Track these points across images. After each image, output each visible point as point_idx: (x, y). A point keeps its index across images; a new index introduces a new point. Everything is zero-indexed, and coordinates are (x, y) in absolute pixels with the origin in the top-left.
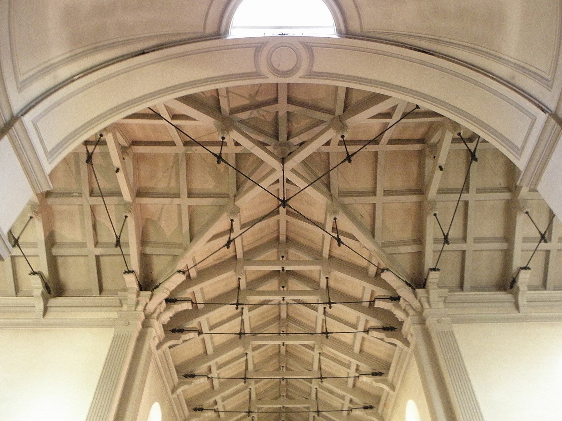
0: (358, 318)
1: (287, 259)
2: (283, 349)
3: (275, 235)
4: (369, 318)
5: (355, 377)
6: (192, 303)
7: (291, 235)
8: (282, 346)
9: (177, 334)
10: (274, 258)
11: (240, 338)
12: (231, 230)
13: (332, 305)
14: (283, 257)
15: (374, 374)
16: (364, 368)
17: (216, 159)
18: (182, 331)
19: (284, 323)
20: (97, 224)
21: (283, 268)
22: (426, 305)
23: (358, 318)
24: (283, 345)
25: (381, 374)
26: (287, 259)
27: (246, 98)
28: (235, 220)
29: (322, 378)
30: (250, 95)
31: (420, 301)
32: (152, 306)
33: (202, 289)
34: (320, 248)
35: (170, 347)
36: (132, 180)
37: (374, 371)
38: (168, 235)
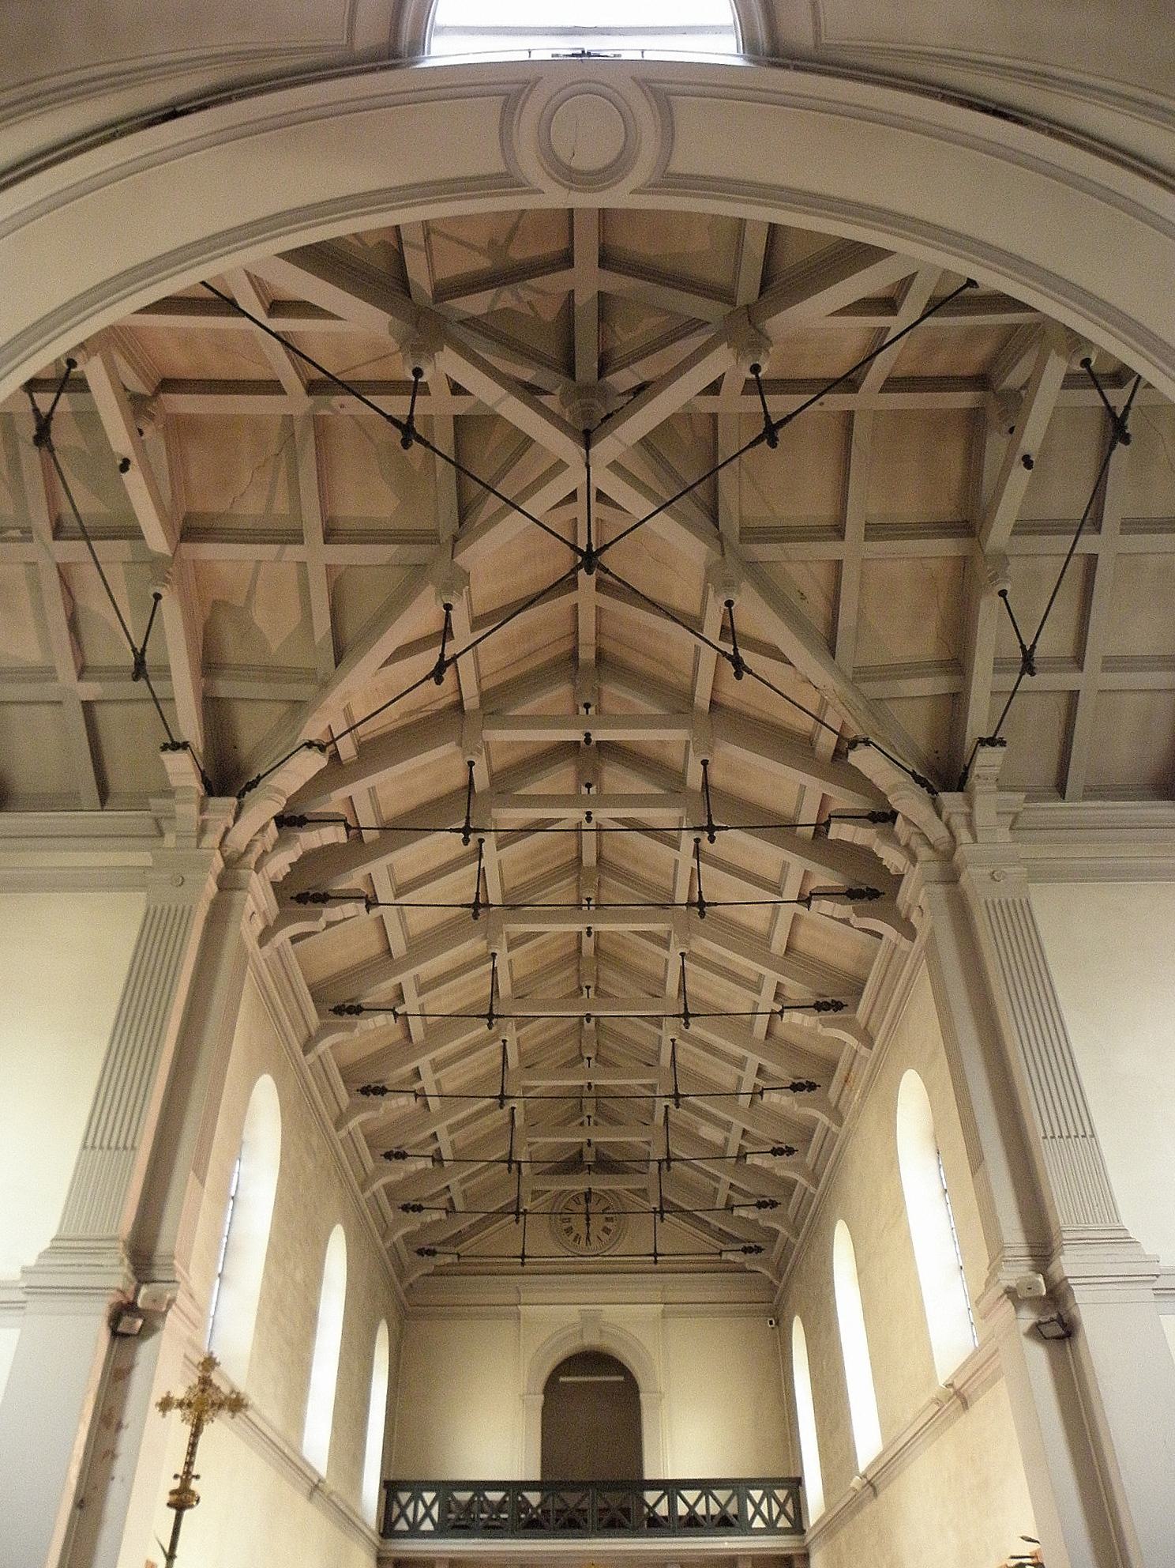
0: (785, 866)
1: (600, 789)
2: (588, 944)
3: (567, 646)
4: (812, 866)
5: (772, 1013)
6: (348, 828)
7: (609, 646)
8: (584, 935)
9: (311, 907)
10: (565, 708)
11: (476, 916)
12: (447, 633)
13: (691, 1020)
14: (587, 706)
15: (819, 1007)
16: (797, 990)
17: (398, 434)
18: (323, 898)
19: (590, 876)
20: (81, 616)
21: (588, 735)
22: (964, 836)
23: (785, 866)
24: (589, 933)
25: (838, 1006)
26: (599, 711)
27: (481, 251)
28: (456, 606)
29: (686, 1015)
30: (492, 243)
31: (948, 826)
32: (241, 835)
33: (372, 791)
34: (687, 681)
35: (294, 939)
36: (167, 494)
37: (821, 1000)
38: (274, 647)
